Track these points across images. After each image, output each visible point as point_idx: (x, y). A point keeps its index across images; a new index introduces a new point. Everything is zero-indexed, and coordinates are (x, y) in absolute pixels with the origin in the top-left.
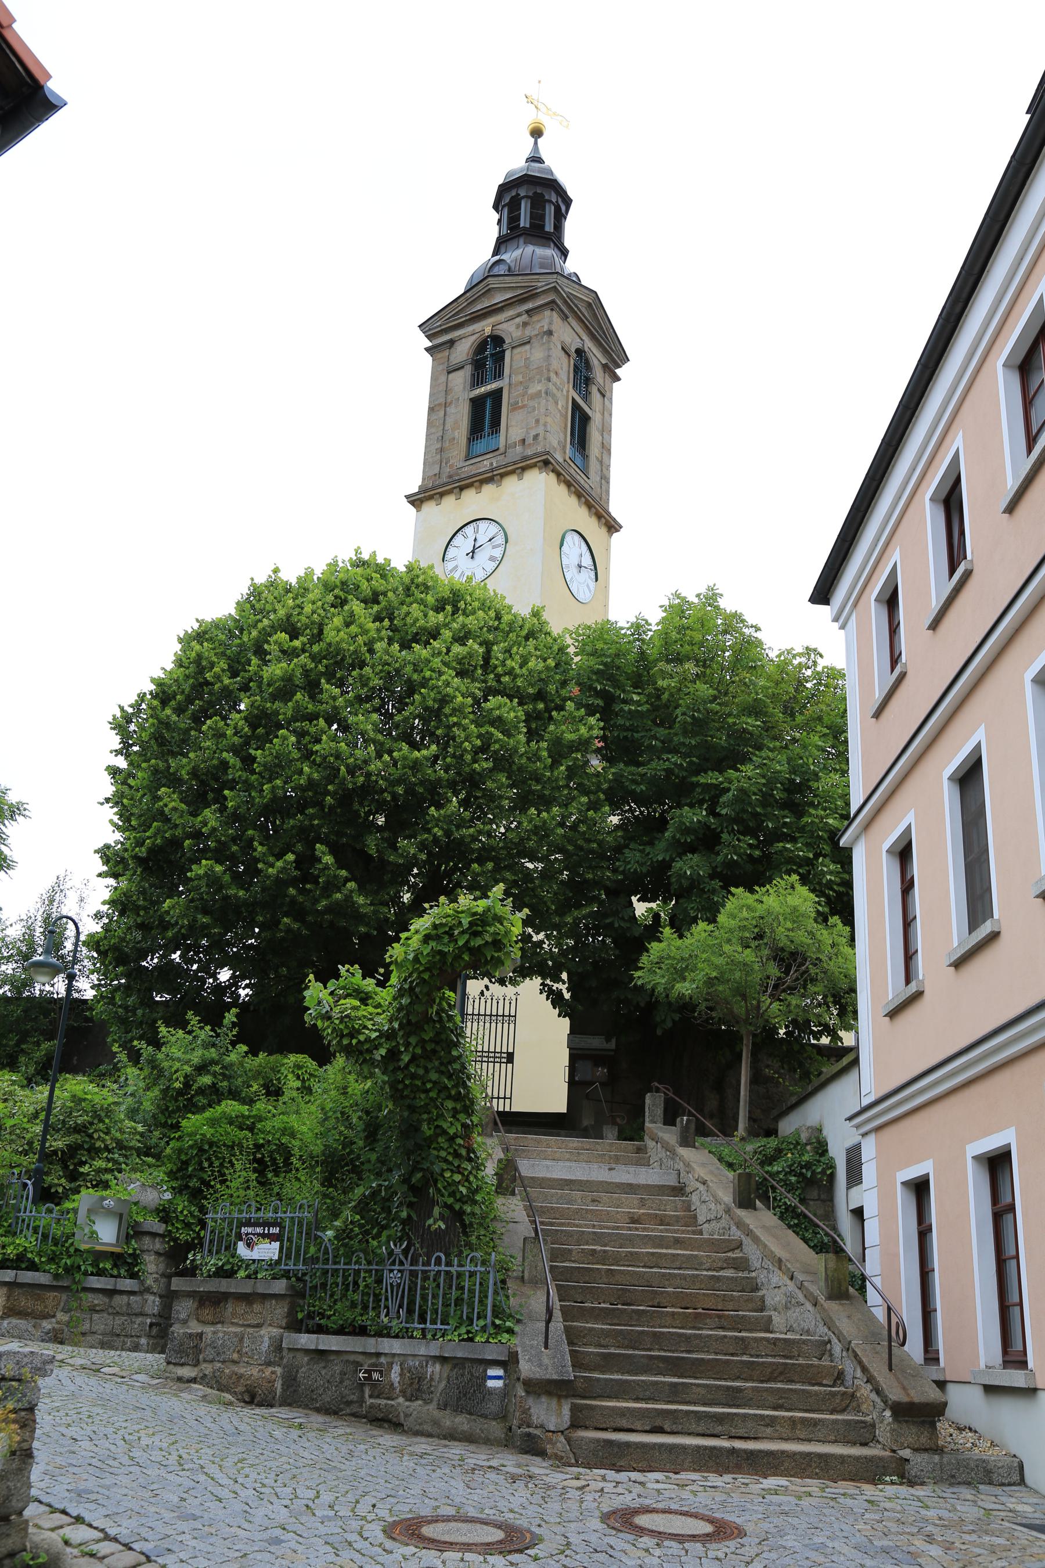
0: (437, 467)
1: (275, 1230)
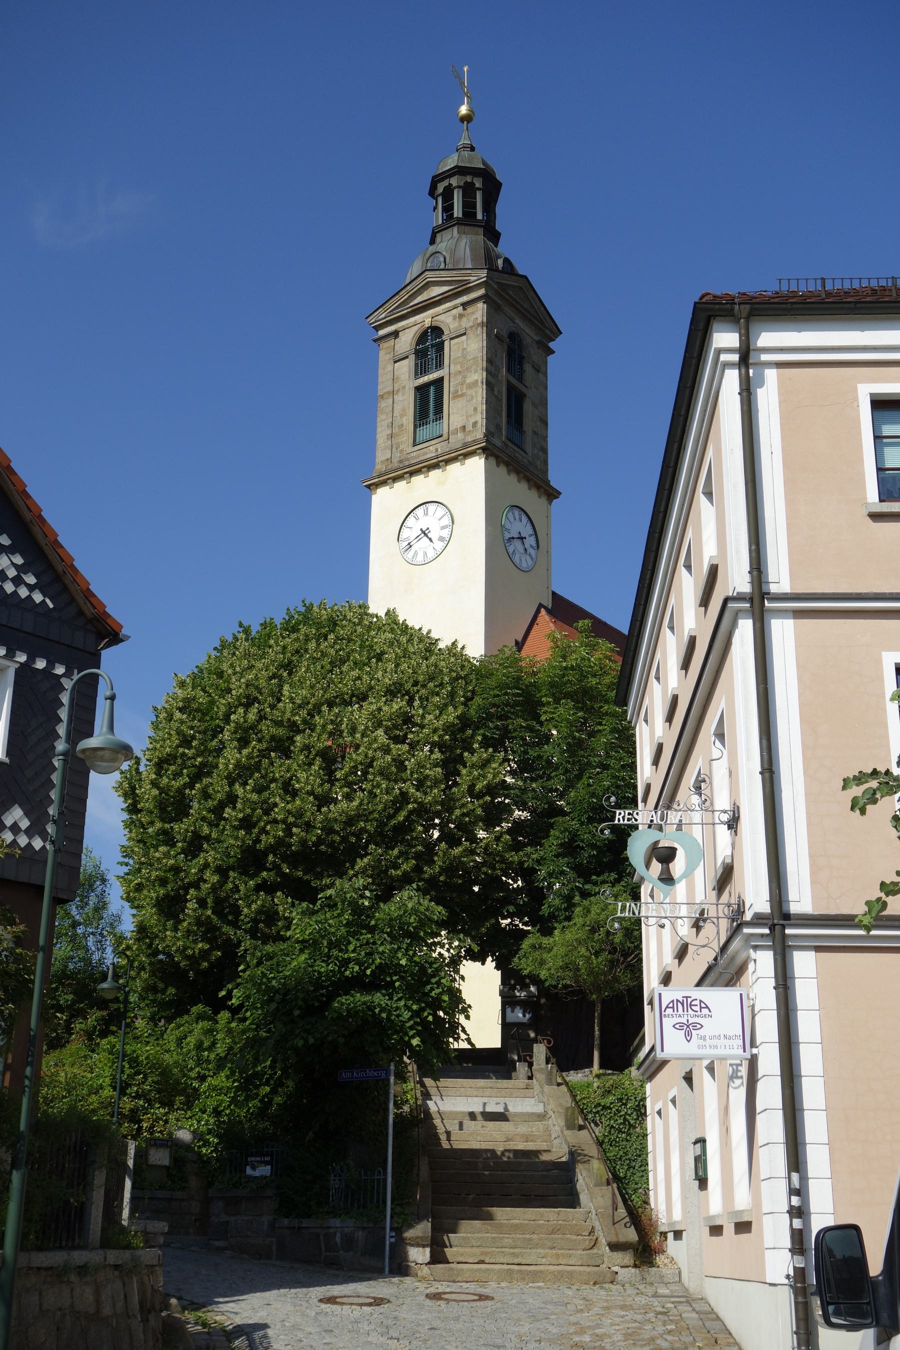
0: (389, 452)
1: (268, 1159)
